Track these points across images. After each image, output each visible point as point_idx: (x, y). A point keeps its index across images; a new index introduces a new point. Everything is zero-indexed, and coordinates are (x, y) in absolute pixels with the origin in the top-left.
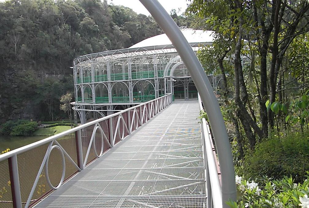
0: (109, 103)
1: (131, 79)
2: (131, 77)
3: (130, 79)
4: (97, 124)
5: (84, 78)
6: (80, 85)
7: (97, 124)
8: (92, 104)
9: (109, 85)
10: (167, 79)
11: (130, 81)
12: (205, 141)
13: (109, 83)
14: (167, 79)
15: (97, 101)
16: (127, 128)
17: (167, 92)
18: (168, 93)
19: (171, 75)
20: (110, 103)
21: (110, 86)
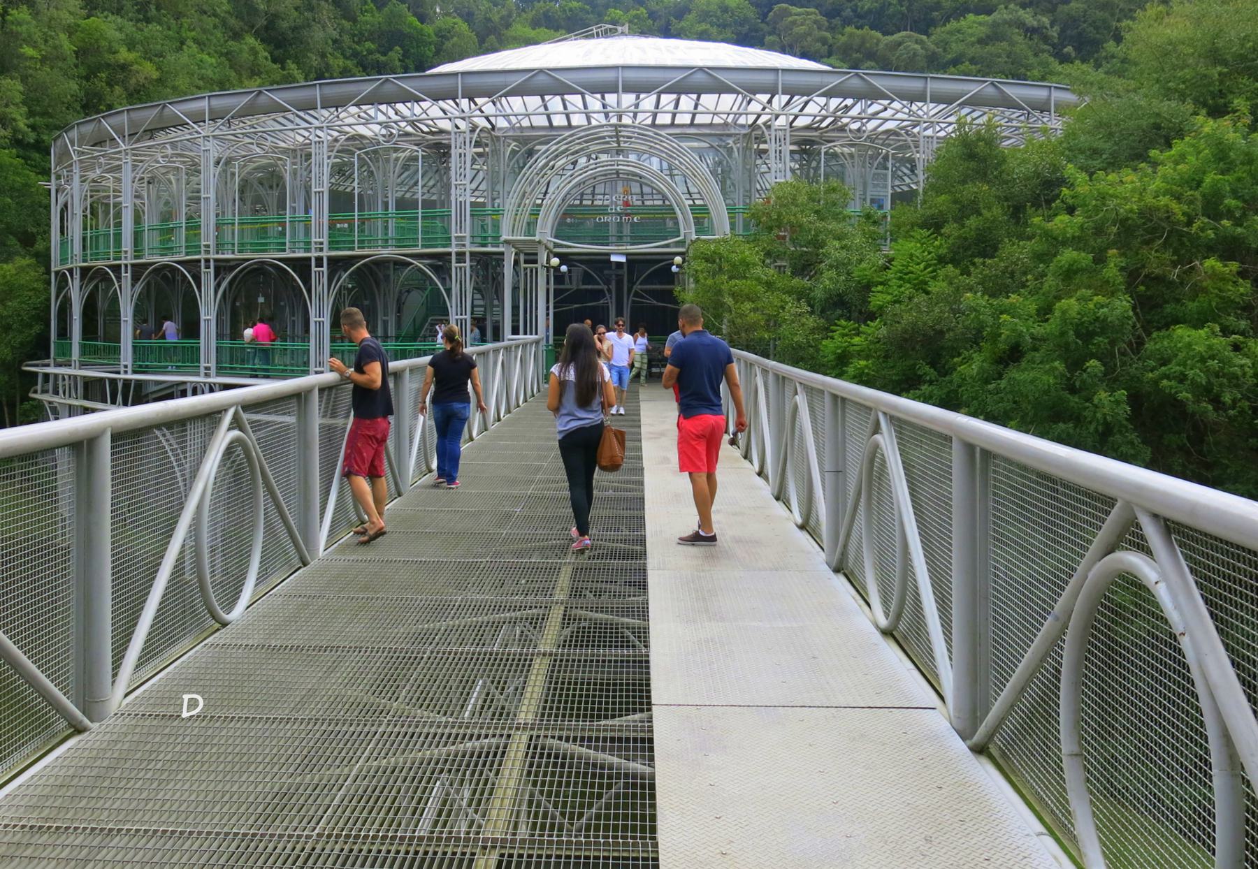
0: (198, 374)
1: (325, 246)
2: (325, 240)
3: (321, 250)
4: (231, 412)
5: (84, 239)
6: (112, 267)
7: (231, 412)
8: (118, 373)
9: (320, 275)
10: (522, 258)
12: (652, 63)
13: (208, 267)
14: (522, 258)
16: (109, 660)
17: (515, 331)
18: (521, 336)
19: (545, 233)
20: (207, 375)
21: (213, 284)
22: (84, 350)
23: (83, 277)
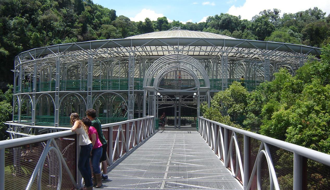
11: (90, 92)
23: (37, 98)
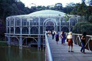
11: (37, 32)
15: (16, 33)
22: (11, 33)
